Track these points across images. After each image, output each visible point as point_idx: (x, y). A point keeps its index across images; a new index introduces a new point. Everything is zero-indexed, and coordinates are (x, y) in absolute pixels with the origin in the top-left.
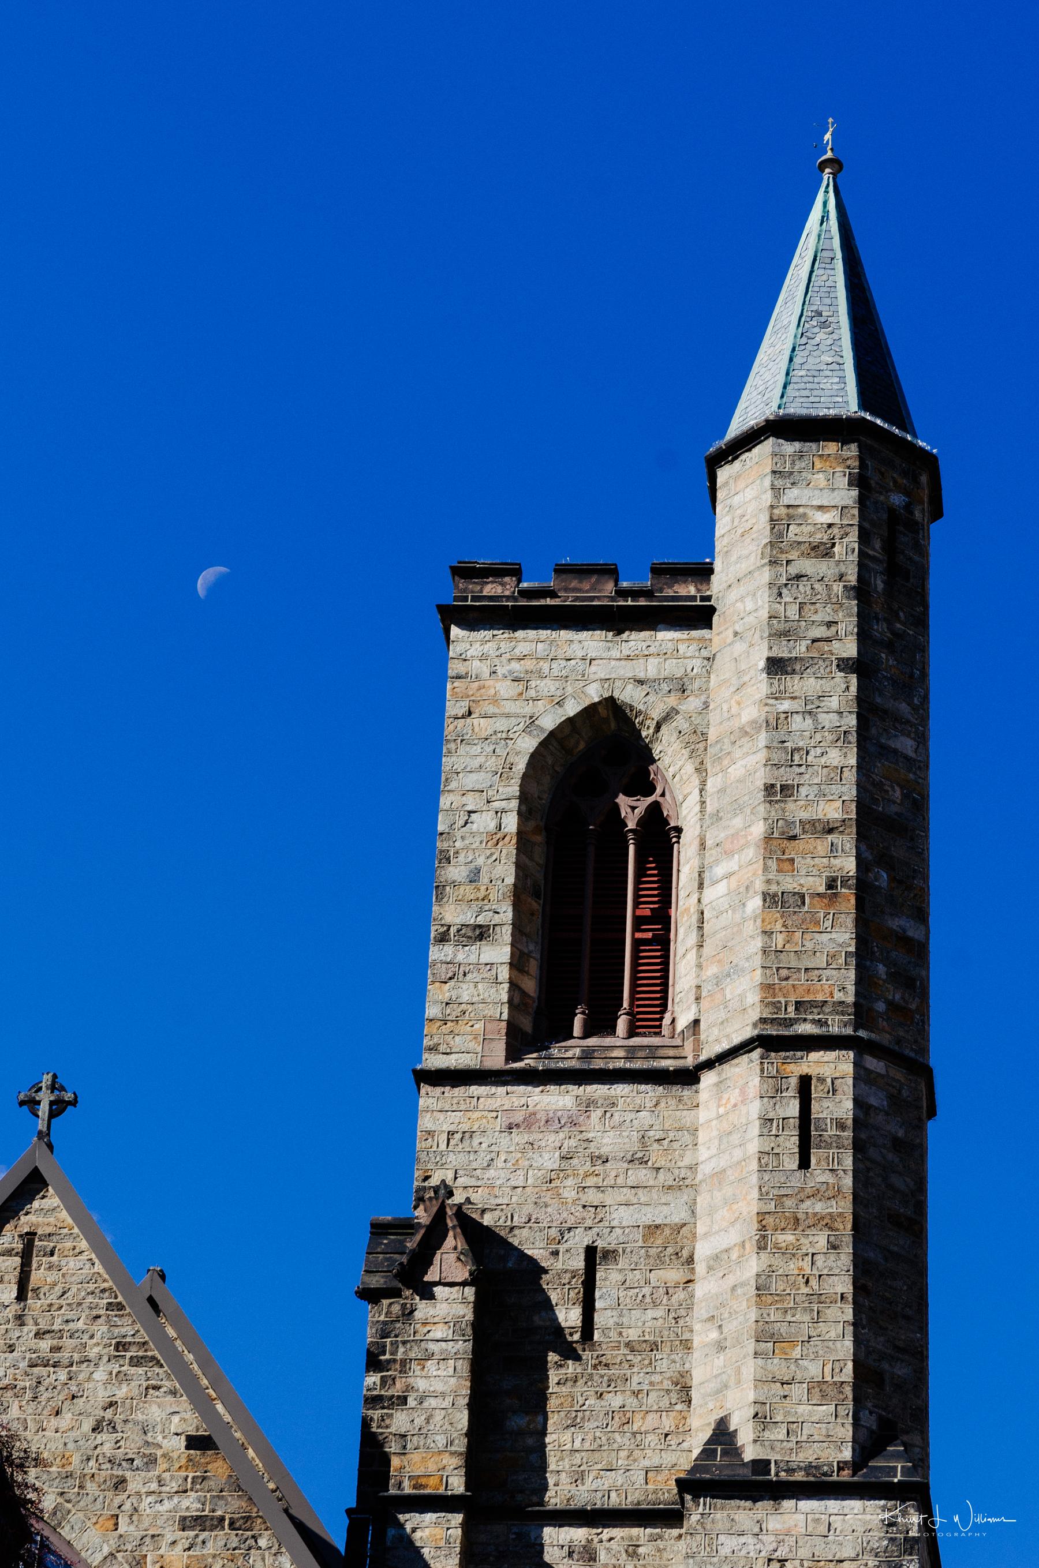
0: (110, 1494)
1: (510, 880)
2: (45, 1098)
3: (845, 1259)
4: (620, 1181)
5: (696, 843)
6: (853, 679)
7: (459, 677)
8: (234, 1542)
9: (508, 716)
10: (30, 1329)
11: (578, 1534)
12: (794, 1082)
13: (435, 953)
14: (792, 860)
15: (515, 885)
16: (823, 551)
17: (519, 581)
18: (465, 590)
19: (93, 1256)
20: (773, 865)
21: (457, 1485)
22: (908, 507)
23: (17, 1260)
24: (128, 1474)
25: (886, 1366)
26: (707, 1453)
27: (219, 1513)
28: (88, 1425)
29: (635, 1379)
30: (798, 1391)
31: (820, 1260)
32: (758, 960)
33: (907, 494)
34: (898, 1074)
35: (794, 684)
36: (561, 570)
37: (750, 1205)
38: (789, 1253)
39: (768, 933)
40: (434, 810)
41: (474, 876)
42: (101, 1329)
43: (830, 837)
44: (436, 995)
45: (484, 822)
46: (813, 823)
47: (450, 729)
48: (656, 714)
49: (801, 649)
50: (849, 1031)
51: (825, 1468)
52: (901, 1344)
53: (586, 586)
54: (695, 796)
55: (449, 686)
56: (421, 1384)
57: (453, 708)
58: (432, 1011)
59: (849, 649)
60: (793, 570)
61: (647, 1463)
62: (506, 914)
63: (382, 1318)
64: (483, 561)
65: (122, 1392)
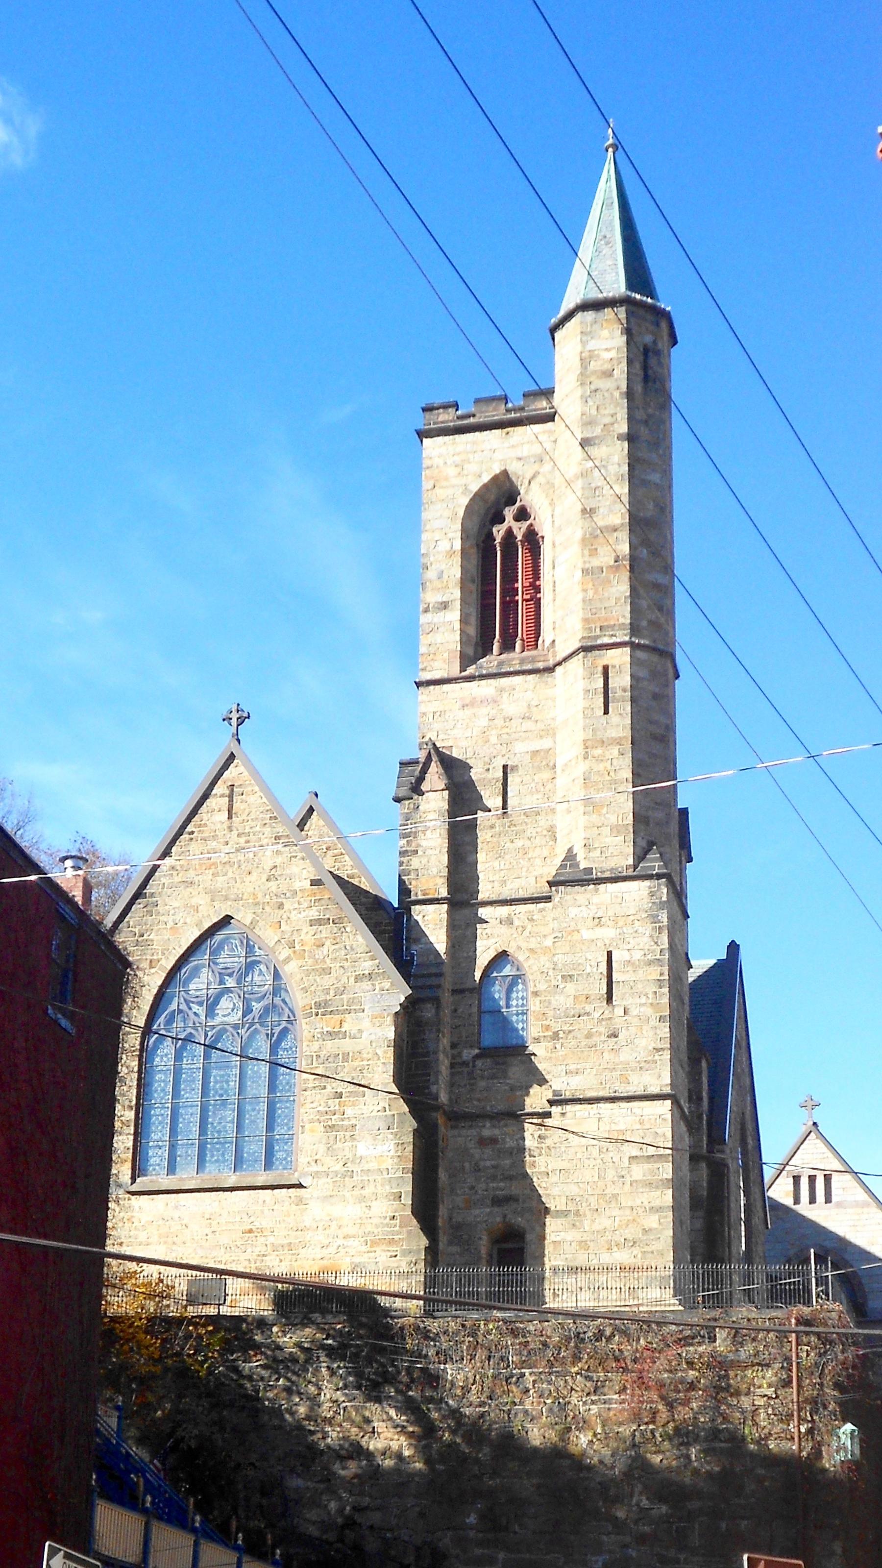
0: (276, 911)
1: (459, 575)
2: (235, 716)
3: (628, 760)
4: (519, 729)
5: (551, 544)
6: (626, 444)
7: (428, 468)
8: (335, 930)
9: (453, 486)
10: (235, 832)
11: (503, 911)
12: (600, 669)
13: (424, 619)
14: (596, 549)
15: (461, 578)
16: (609, 374)
17: (457, 410)
18: (429, 420)
19: (262, 795)
20: (586, 552)
21: (444, 893)
22: (655, 342)
23: (227, 799)
24: (284, 901)
25: (650, 813)
26: (563, 866)
27: (327, 916)
28: (264, 877)
29: (529, 831)
30: (606, 831)
31: (615, 762)
32: (581, 605)
33: (653, 333)
34: (655, 658)
35: (594, 451)
36: (477, 401)
37: (580, 736)
38: (599, 760)
39: (585, 591)
40: (418, 542)
41: (440, 576)
42: (267, 830)
43: (615, 534)
44: (424, 640)
45: (444, 546)
46: (607, 527)
47: (425, 497)
48: (528, 476)
49: (598, 431)
50: (627, 639)
51: (620, 869)
52: (659, 801)
53: (491, 409)
54: (550, 519)
55: (423, 473)
56: (424, 843)
57: (426, 485)
58: (423, 649)
59: (624, 428)
60: (593, 387)
61: (536, 873)
62: (457, 593)
63: (406, 811)
64: (437, 402)
65: (279, 860)
